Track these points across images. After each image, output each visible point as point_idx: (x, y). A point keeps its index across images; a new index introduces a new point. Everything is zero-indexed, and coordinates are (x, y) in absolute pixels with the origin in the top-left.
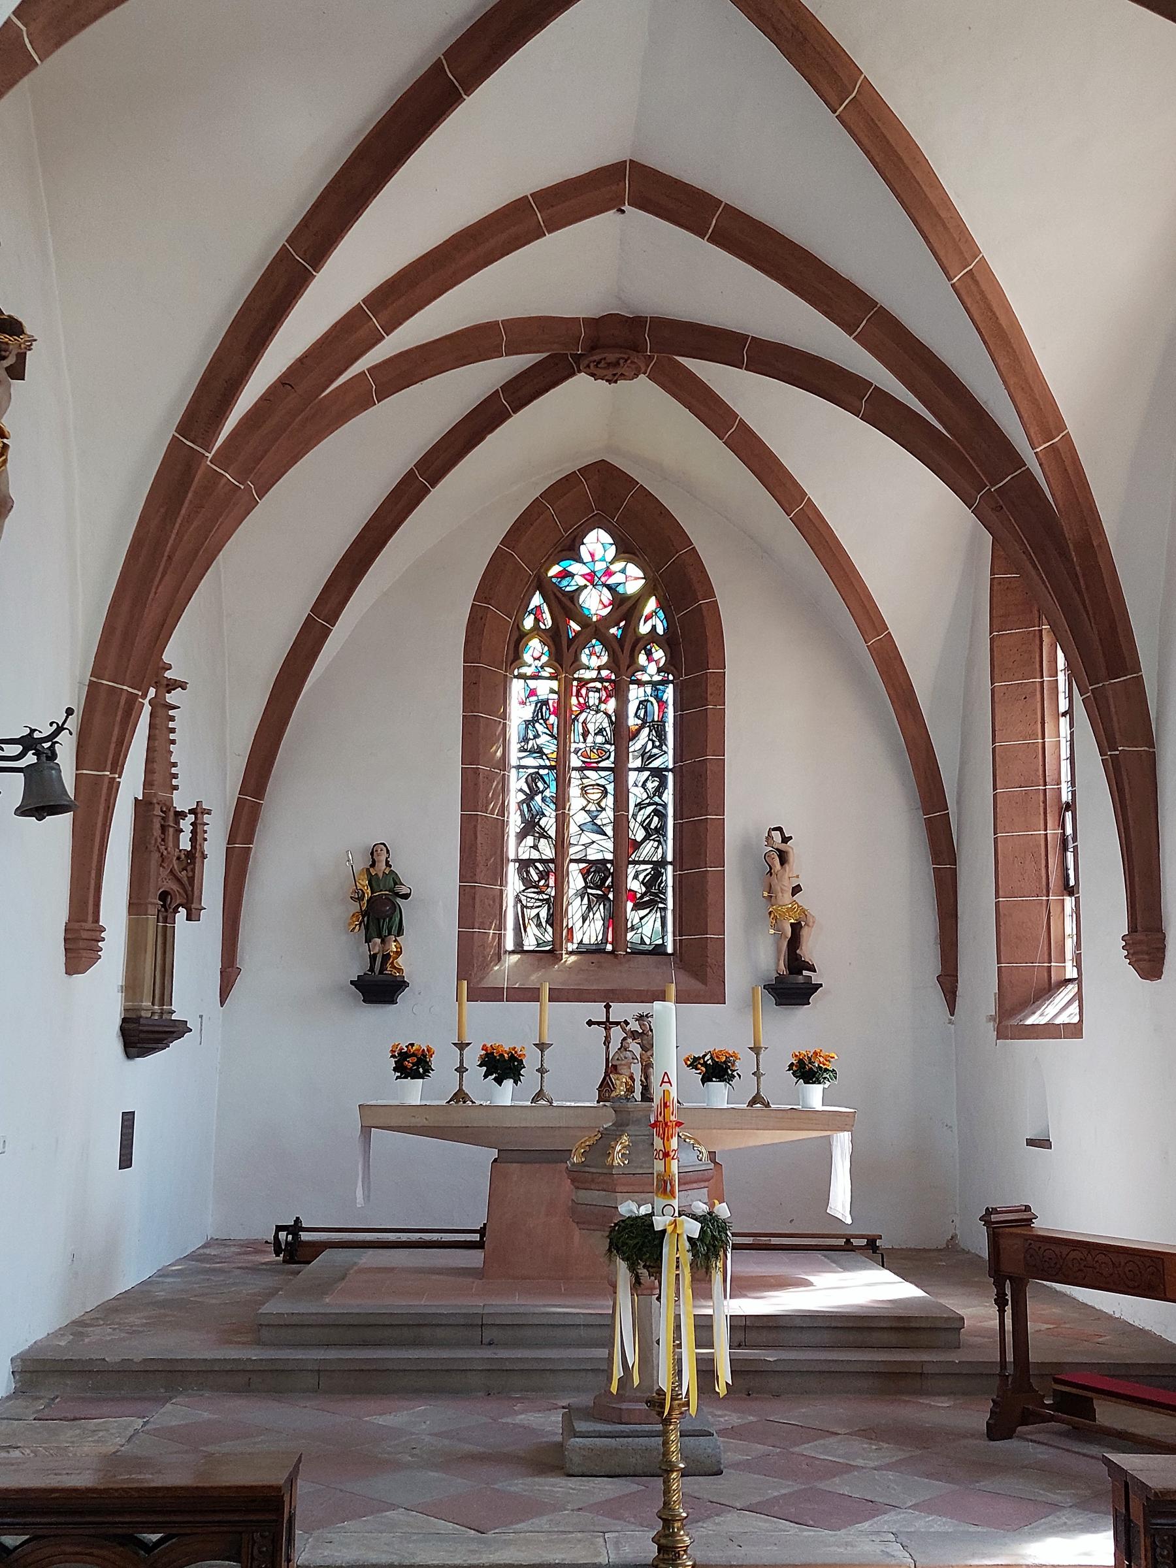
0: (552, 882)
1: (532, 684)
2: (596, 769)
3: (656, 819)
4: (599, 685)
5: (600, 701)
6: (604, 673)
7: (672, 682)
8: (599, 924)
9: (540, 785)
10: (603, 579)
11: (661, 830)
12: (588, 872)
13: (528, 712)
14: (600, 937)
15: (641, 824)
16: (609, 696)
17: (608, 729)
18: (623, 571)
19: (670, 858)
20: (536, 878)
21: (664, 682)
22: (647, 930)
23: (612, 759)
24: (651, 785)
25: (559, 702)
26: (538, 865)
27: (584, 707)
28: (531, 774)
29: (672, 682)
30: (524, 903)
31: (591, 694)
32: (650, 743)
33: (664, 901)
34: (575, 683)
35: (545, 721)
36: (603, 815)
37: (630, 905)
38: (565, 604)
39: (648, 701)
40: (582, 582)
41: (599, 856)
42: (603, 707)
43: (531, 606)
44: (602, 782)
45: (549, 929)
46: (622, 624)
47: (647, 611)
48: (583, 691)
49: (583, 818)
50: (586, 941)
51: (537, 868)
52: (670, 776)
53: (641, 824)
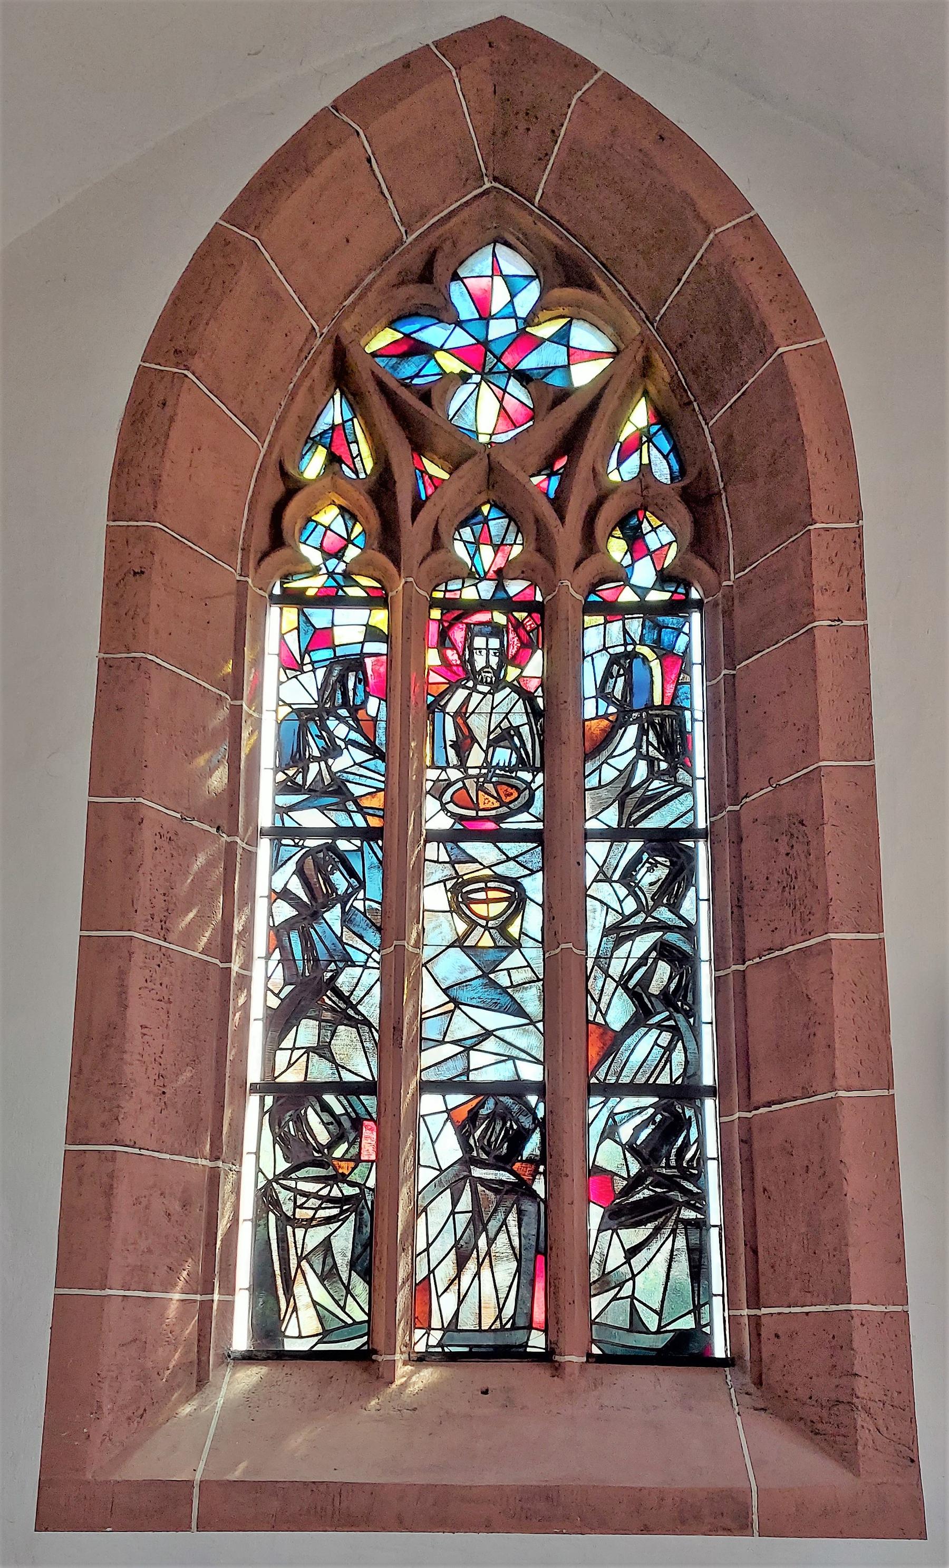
0: (368, 1149)
1: (320, 617)
2: (495, 837)
3: (664, 969)
4: (500, 618)
5: (505, 660)
6: (514, 588)
7: (699, 605)
8: (505, 1270)
9: (340, 881)
10: (508, 359)
11: (680, 999)
12: (473, 1117)
13: (304, 690)
14: (509, 1311)
15: (623, 982)
16: (528, 646)
17: (525, 730)
18: (562, 337)
19: (708, 1078)
20: (323, 1137)
21: (679, 607)
22: (649, 1286)
23: (537, 808)
24: (649, 878)
25: (389, 663)
26: (330, 1099)
27: (462, 674)
28: (312, 852)
29: (699, 605)
30: (288, 1208)
31: (479, 642)
32: (642, 767)
33: (698, 1201)
34: (436, 614)
35: (354, 710)
36: (515, 959)
37: (596, 1213)
38: (412, 417)
39: (635, 655)
40: (453, 365)
41: (503, 1073)
42: (512, 673)
43: (323, 424)
44: (511, 870)
45: (360, 1287)
46: (559, 464)
47: (627, 431)
48: (458, 635)
49: (454, 966)
50: (467, 1321)
51: (326, 1108)
52: (702, 850)
53: (623, 982)
